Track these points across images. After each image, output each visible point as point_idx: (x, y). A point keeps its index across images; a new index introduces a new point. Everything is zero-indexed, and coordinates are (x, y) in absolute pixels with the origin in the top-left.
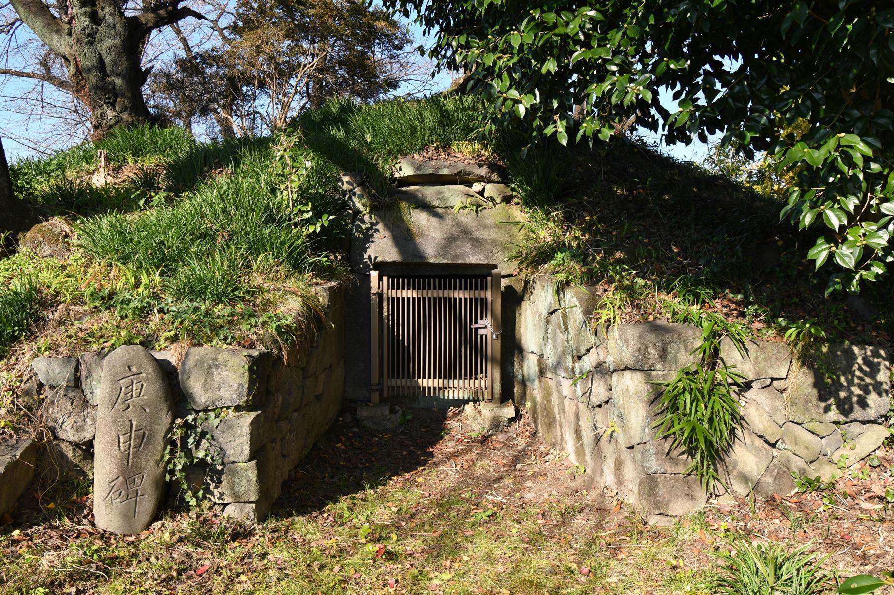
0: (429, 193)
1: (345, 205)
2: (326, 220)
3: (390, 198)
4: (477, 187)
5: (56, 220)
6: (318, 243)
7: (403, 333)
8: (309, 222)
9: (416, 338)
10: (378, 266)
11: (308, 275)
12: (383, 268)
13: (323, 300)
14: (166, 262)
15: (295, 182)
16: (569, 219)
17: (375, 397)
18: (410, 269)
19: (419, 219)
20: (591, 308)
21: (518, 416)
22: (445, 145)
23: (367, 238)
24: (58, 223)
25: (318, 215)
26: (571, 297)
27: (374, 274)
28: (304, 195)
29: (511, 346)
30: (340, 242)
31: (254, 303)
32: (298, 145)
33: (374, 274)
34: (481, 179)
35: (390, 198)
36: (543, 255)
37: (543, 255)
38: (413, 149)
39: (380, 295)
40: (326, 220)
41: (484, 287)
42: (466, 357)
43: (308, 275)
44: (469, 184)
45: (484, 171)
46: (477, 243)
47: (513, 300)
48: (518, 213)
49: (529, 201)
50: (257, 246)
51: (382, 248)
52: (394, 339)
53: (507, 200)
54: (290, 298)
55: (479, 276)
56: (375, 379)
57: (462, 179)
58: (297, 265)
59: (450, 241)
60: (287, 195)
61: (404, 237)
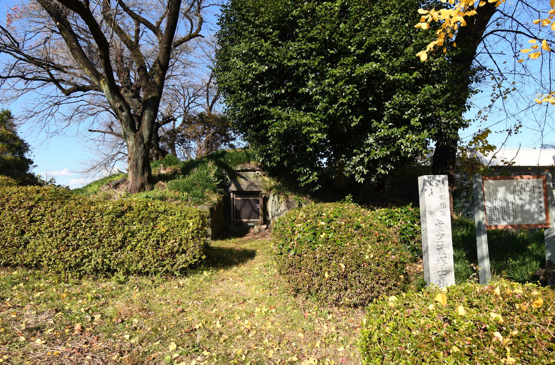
0: (244, 174)
1: (224, 177)
2: (220, 181)
3: (234, 175)
4: (257, 172)
5: (161, 182)
6: (220, 186)
7: (238, 208)
8: (217, 181)
9: (241, 209)
10: (233, 192)
11: (217, 193)
12: (234, 192)
13: (221, 199)
14: (187, 190)
15: (213, 172)
16: (278, 180)
17: (232, 224)
18: (240, 192)
19: (242, 181)
20: (279, 199)
21: (267, 228)
22: (249, 162)
23: (230, 185)
24: (161, 182)
25: (218, 180)
26: (276, 197)
27: (232, 194)
28: (215, 175)
29: (266, 213)
30: (224, 186)
31: (208, 198)
32: (214, 164)
33: (232, 194)
34: (258, 170)
35: (234, 175)
36: (271, 189)
37: (271, 189)
38: (241, 163)
39: (233, 199)
40: (220, 181)
41: (258, 197)
42: (255, 213)
43: (217, 193)
44: (255, 171)
45: (258, 168)
46: (256, 186)
47: (266, 200)
48: (266, 179)
49: (269, 176)
50: (206, 187)
51: (233, 188)
52: (236, 210)
53: (264, 175)
54: (215, 198)
55: (257, 194)
56: (232, 219)
57: (253, 170)
58: (215, 191)
59: (249, 186)
60: (212, 175)
61: (238, 185)
